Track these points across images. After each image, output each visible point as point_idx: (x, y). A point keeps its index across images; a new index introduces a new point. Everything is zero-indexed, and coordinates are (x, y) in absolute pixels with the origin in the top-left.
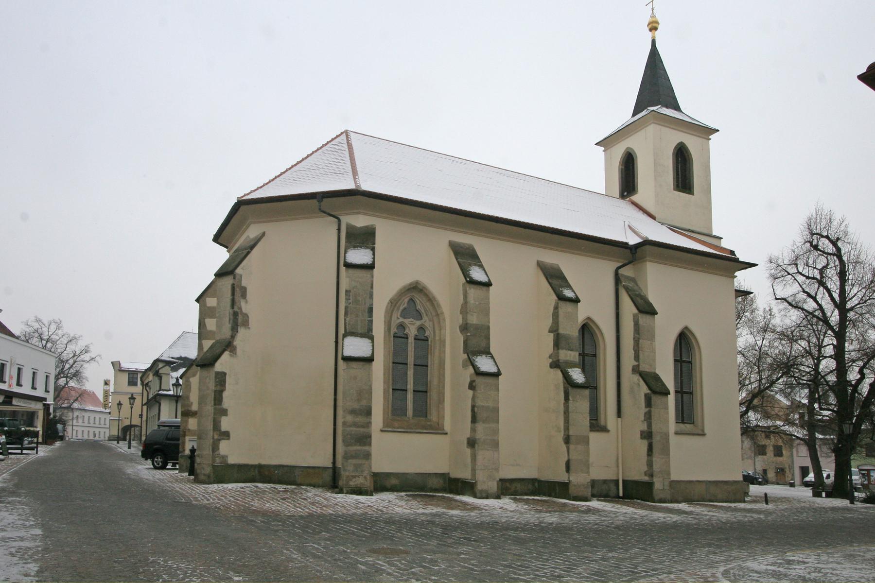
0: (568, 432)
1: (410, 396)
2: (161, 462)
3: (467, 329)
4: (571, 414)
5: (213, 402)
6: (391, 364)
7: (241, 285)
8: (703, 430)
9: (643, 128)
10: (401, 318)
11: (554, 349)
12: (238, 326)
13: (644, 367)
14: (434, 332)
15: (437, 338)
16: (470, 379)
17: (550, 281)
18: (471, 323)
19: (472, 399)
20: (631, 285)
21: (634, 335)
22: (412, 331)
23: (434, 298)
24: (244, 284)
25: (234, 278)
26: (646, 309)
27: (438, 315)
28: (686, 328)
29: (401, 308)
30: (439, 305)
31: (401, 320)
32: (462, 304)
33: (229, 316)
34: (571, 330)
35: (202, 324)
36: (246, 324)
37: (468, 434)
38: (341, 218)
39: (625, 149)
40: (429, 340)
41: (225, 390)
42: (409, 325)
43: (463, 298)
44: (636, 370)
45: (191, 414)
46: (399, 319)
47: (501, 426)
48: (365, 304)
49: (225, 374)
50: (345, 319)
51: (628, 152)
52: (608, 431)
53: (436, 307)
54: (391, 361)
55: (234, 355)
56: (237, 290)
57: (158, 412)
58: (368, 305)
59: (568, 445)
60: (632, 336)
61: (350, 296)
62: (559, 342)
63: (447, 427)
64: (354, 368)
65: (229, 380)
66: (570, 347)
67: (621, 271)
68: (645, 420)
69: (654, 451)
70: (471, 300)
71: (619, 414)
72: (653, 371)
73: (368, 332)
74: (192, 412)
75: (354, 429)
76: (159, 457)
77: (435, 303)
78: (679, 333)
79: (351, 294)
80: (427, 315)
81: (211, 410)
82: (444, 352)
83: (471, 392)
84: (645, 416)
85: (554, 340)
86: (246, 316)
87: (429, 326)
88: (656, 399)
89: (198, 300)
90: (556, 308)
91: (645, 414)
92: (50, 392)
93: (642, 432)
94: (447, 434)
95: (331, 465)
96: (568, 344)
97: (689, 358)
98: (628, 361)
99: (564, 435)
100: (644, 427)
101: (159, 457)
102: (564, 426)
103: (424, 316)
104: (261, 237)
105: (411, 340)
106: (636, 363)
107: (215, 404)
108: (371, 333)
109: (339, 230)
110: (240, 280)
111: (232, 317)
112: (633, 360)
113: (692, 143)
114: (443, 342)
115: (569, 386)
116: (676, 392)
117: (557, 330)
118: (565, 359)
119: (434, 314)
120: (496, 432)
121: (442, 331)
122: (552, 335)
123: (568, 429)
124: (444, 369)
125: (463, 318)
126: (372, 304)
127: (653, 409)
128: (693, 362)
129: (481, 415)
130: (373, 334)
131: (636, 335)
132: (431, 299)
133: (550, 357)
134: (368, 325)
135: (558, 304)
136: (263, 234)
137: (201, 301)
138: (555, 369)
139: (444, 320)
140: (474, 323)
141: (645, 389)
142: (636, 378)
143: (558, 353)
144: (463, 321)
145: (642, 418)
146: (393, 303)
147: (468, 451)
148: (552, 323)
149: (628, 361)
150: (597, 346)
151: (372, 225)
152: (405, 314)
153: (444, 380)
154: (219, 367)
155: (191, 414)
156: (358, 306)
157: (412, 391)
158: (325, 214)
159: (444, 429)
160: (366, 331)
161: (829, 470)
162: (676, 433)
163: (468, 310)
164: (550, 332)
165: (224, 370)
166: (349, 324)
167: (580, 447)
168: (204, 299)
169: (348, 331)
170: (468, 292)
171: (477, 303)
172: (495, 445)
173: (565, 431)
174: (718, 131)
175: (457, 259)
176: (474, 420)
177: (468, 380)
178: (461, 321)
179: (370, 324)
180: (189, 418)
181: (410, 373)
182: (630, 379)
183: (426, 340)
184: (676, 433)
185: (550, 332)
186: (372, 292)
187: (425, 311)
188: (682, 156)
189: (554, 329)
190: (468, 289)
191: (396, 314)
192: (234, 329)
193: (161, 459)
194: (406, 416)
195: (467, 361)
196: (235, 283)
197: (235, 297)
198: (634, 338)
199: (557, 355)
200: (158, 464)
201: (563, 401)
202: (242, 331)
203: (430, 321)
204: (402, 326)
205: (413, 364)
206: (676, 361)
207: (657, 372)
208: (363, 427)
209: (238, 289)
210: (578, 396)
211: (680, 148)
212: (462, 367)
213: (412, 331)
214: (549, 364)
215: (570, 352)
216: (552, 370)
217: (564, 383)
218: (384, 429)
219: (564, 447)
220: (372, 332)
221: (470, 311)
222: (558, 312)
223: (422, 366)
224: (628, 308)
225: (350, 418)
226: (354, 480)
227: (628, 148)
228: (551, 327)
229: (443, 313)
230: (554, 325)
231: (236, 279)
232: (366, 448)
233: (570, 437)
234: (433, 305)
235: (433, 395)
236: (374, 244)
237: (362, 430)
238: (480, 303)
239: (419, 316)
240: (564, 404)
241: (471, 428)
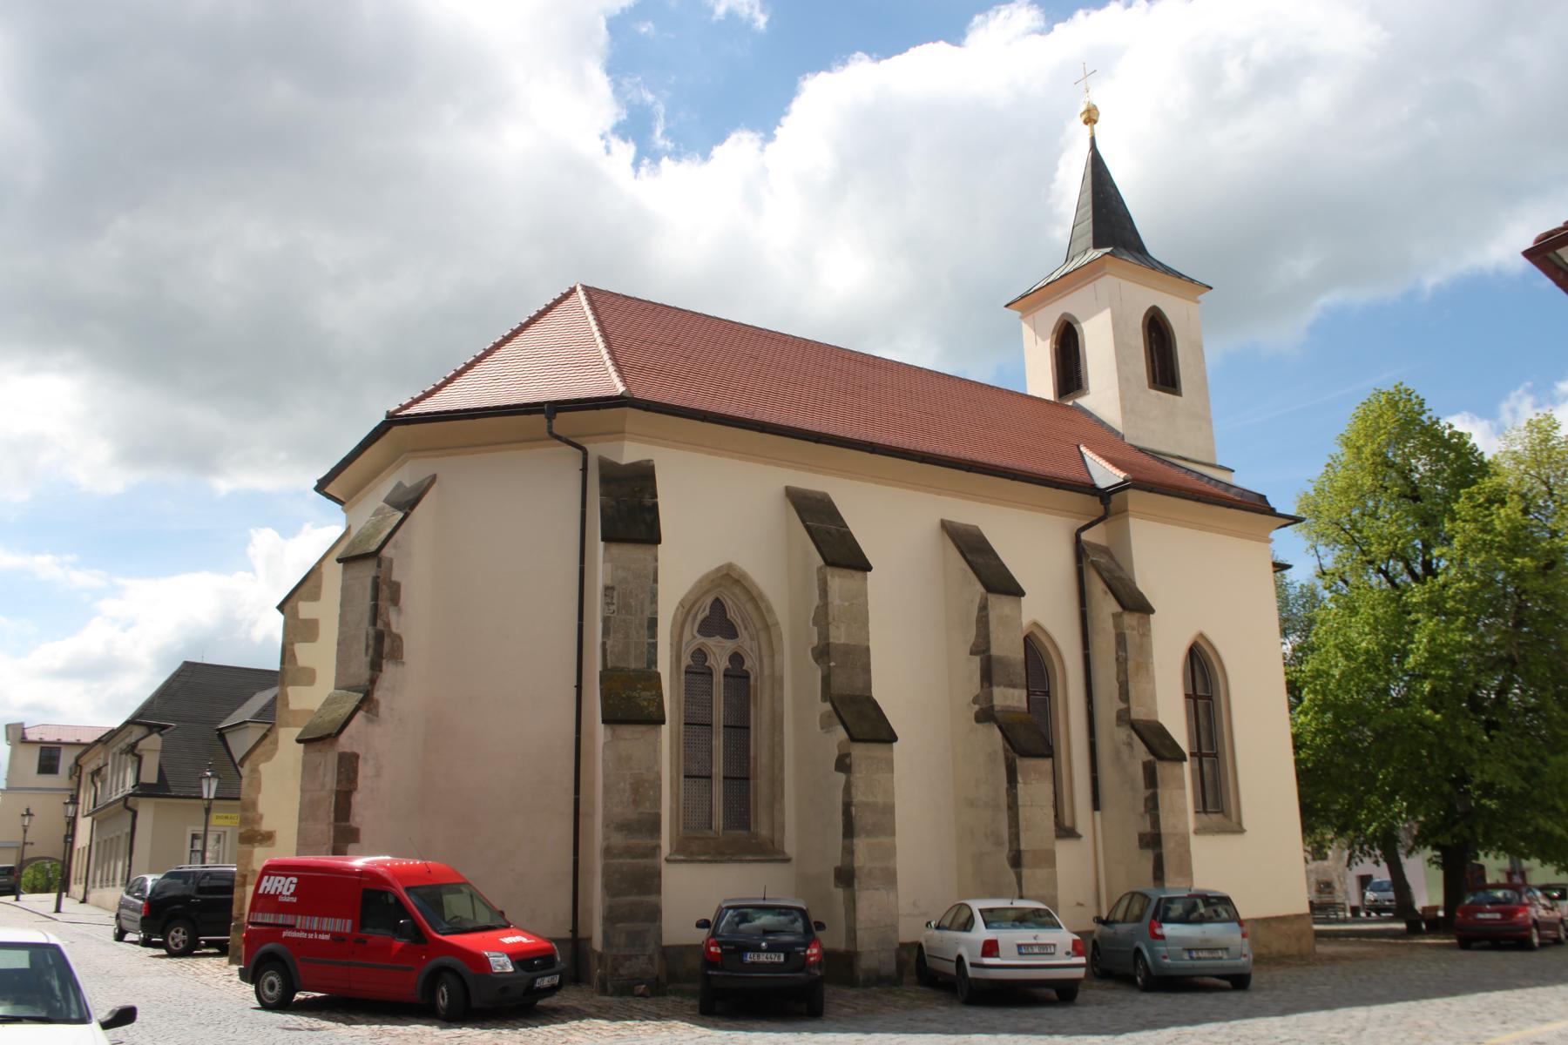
0: (1019, 845)
1: (718, 788)
2: (184, 942)
3: (828, 654)
4: (1021, 810)
5: (332, 815)
6: (682, 727)
7: (390, 578)
8: (1240, 823)
9: (1091, 282)
10: (699, 636)
11: (982, 687)
12: (382, 658)
13: (1138, 713)
14: (761, 661)
15: (766, 672)
16: (839, 751)
17: (969, 557)
18: (837, 642)
19: (844, 790)
20: (1103, 560)
21: (1117, 653)
22: (719, 661)
23: (761, 595)
24: (395, 577)
25: (379, 566)
26: (1137, 605)
27: (767, 628)
28: (1201, 635)
29: (700, 617)
30: (770, 610)
31: (700, 639)
32: (818, 607)
33: (367, 639)
34: (1007, 647)
35: (288, 654)
36: (397, 655)
37: (836, 857)
38: (590, 447)
39: (1059, 315)
40: (752, 677)
41: (355, 789)
42: (714, 649)
43: (820, 595)
44: (1124, 718)
45: (259, 838)
46: (694, 637)
47: (900, 840)
48: (642, 612)
49: (356, 757)
50: (604, 644)
51: (1065, 320)
52: (1078, 836)
53: (764, 610)
54: (682, 722)
55: (375, 718)
56: (384, 589)
57: (128, 829)
58: (647, 614)
59: (1018, 870)
60: (1114, 656)
61: (612, 598)
62: (989, 672)
63: (790, 848)
64: (625, 739)
65: (365, 771)
66: (1012, 681)
67: (1085, 536)
68: (1146, 812)
69: (1166, 869)
70: (835, 600)
71: (1096, 804)
72: (1152, 718)
73: (649, 666)
74: (261, 834)
75: (628, 860)
76: (182, 930)
77: (763, 606)
78: (1188, 648)
79: (615, 594)
80: (746, 628)
81: (329, 831)
82: (782, 699)
83: (842, 777)
84: (1146, 806)
85: (981, 669)
86: (397, 639)
87: (752, 651)
88: (1163, 769)
89: (281, 607)
90: (983, 608)
91: (1146, 800)
92: (279, 838)
93: (1142, 837)
94: (787, 860)
95: (568, 935)
96: (1008, 676)
97: (1207, 691)
98: (1107, 708)
99: (1010, 850)
100: (1147, 827)
101: (182, 930)
102: (1010, 835)
103: (742, 632)
104: (429, 484)
105: (718, 678)
106: (1123, 706)
107: (336, 819)
108: (653, 668)
109: (584, 470)
110: (390, 569)
111: (371, 642)
112: (1118, 701)
113: (1176, 311)
114: (777, 682)
115: (1017, 755)
116: (1192, 754)
117: (988, 649)
118: (1003, 704)
119: (759, 625)
120: (891, 852)
121: (776, 657)
122: (977, 659)
123: (1018, 839)
124: (782, 732)
125: (819, 634)
126: (656, 612)
127: (1159, 791)
128: (1214, 698)
129: (862, 819)
130: (659, 670)
131: (1120, 653)
132: (755, 598)
133: (975, 701)
134: (649, 652)
135: (987, 599)
136: (433, 479)
137: (287, 608)
138: (986, 724)
139: (780, 636)
140: (842, 641)
141: (1142, 753)
142: (1123, 733)
143: (991, 693)
144: (819, 639)
145: (1142, 809)
146: (687, 608)
147: (839, 894)
148: (977, 636)
149: (1107, 708)
150: (1050, 677)
151: (649, 461)
152: (707, 628)
153: (783, 756)
154: (345, 743)
155: (259, 838)
156: (629, 617)
157: (721, 779)
158: (558, 442)
159: (784, 853)
160: (645, 666)
161: (1427, 891)
162: (1197, 832)
163: (830, 619)
164: (972, 653)
165: (355, 749)
166: (611, 652)
167: (1041, 873)
168: (294, 604)
169: (609, 666)
170: (829, 583)
171: (847, 604)
172: (890, 878)
173: (1011, 842)
174: (1211, 288)
175: (803, 521)
176: (849, 830)
177: (835, 754)
178: (815, 640)
179: (653, 651)
180: (254, 847)
181: (718, 742)
182: (1111, 734)
183: (747, 676)
184: (1197, 832)
185: (972, 653)
186: (657, 589)
187: (743, 621)
188: (1158, 332)
189: (981, 647)
190: (829, 578)
191: (690, 631)
192: (376, 666)
193: (184, 934)
194: (711, 828)
195: (829, 716)
196: (379, 575)
197: (379, 603)
198: (1117, 659)
199: (990, 698)
200: (177, 945)
201: (1005, 785)
202: (389, 669)
203: (752, 639)
204: (700, 654)
205: (722, 725)
206: (1187, 696)
207: (1161, 720)
208: (645, 856)
209: (384, 587)
210: (1033, 774)
211: (1153, 317)
212: (819, 729)
213: (719, 661)
214: (973, 715)
215: (1011, 691)
216: (980, 727)
217: (1006, 750)
218: (672, 858)
219: (1011, 874)
220: (656, 667)
221: (834, 619)
222: (987, 616)
223: (739, 729)
224: (1105, 606)
225: (618, 839)
226: (627, 964)
227: (1064, 315)
228: (974, 644)
229: (778, 624)
230: (980, 640)
231: (383, 567)
232: (651, 898)
233: (1023, 854)
234: (757, 608)
235: (761, 785)
236: (656, 496)
237: (642, 861)
238: (853, 604)
239: (730, 632)
240: (1007, 790)
241: (844, 848)
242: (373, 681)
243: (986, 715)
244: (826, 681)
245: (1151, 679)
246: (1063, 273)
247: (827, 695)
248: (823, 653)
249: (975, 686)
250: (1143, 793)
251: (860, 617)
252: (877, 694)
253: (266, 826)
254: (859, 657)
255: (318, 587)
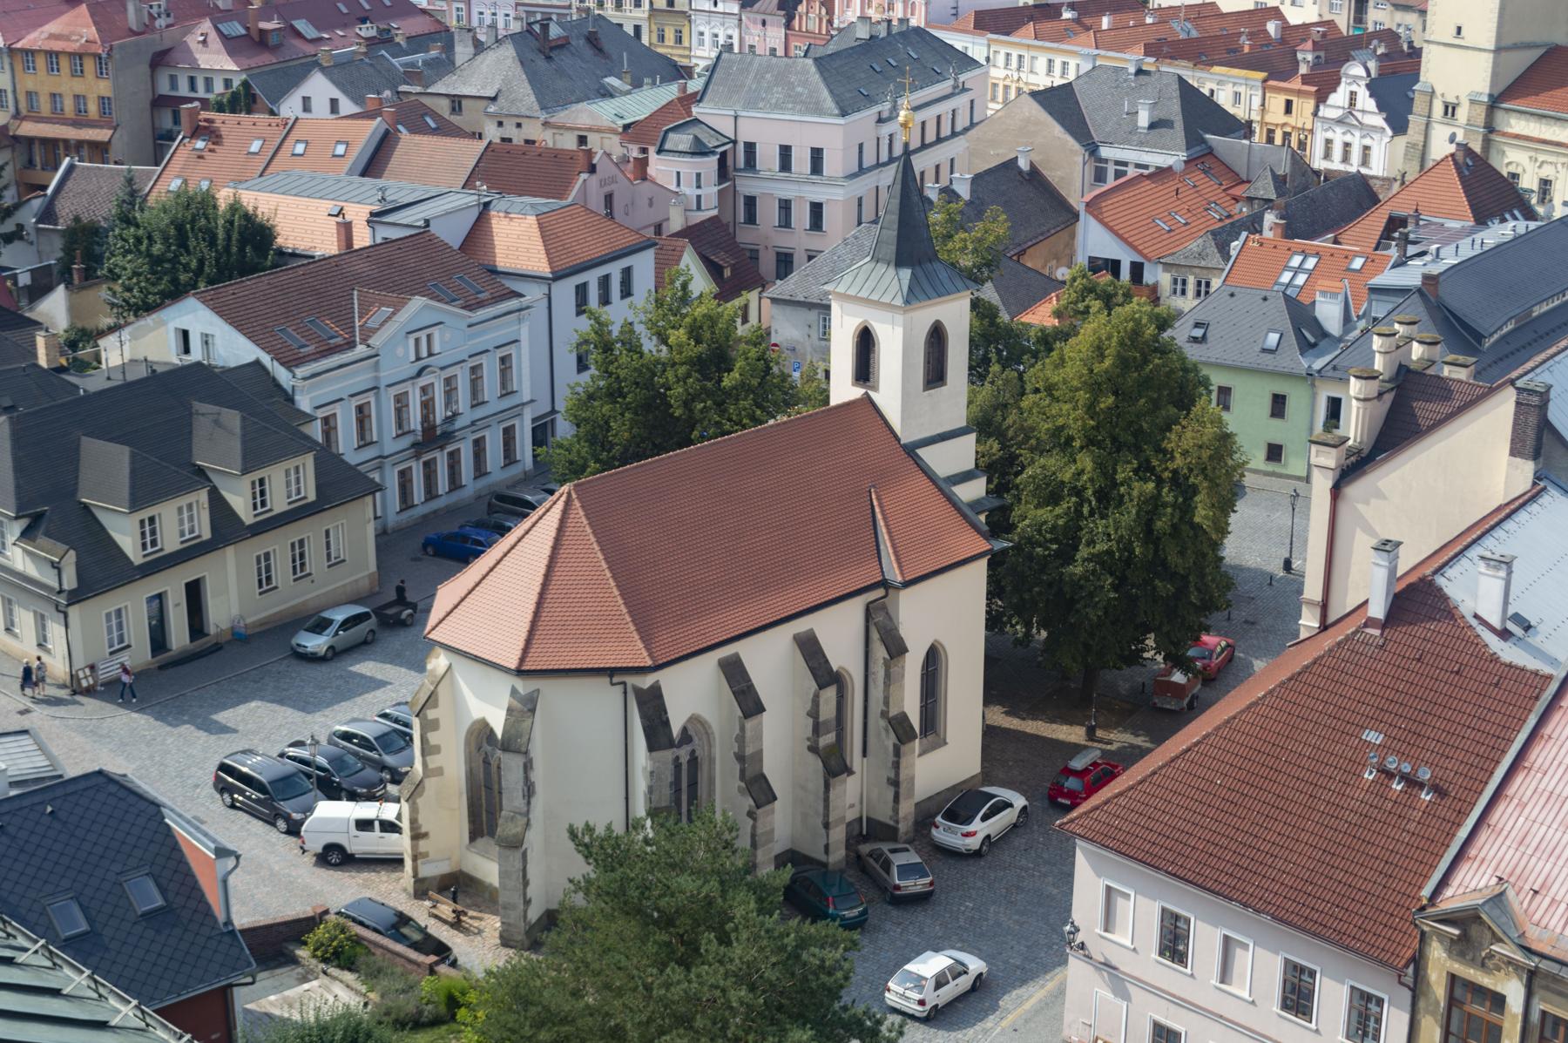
8: (945, 739)
30: (710, 727)
44: (884, 714)
62: (817, 729)
71: (865, 754)
98: (876, 706)
103: (696, 739)
114: (712, 761)
142: (883, 723)
149: (876, 706)
182: (876, 722)
219: (823, 831)
223: (693, 784)
242: (528, 811)
243: (813, 749)
244: (742, 772)
245: (902, 687)
246: (882, 547)
247: (742, 777)
248: (740, 758)
249: (809, 732)
250: (891, 758)
251: (759, 737)
252: (766, 771)
253: (423, 830)
254: (758, 755)
255: (437, 700)
